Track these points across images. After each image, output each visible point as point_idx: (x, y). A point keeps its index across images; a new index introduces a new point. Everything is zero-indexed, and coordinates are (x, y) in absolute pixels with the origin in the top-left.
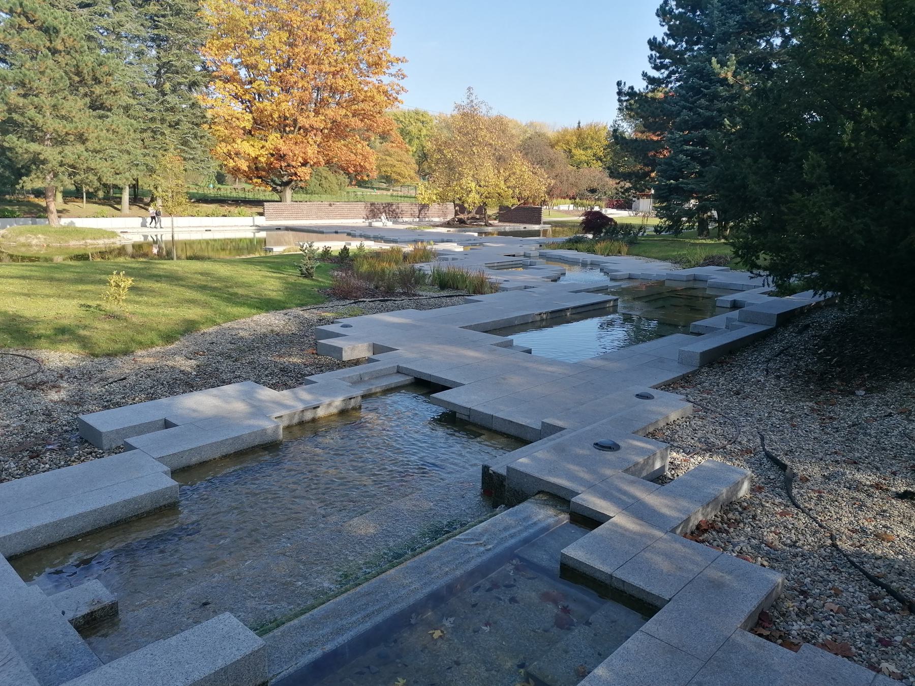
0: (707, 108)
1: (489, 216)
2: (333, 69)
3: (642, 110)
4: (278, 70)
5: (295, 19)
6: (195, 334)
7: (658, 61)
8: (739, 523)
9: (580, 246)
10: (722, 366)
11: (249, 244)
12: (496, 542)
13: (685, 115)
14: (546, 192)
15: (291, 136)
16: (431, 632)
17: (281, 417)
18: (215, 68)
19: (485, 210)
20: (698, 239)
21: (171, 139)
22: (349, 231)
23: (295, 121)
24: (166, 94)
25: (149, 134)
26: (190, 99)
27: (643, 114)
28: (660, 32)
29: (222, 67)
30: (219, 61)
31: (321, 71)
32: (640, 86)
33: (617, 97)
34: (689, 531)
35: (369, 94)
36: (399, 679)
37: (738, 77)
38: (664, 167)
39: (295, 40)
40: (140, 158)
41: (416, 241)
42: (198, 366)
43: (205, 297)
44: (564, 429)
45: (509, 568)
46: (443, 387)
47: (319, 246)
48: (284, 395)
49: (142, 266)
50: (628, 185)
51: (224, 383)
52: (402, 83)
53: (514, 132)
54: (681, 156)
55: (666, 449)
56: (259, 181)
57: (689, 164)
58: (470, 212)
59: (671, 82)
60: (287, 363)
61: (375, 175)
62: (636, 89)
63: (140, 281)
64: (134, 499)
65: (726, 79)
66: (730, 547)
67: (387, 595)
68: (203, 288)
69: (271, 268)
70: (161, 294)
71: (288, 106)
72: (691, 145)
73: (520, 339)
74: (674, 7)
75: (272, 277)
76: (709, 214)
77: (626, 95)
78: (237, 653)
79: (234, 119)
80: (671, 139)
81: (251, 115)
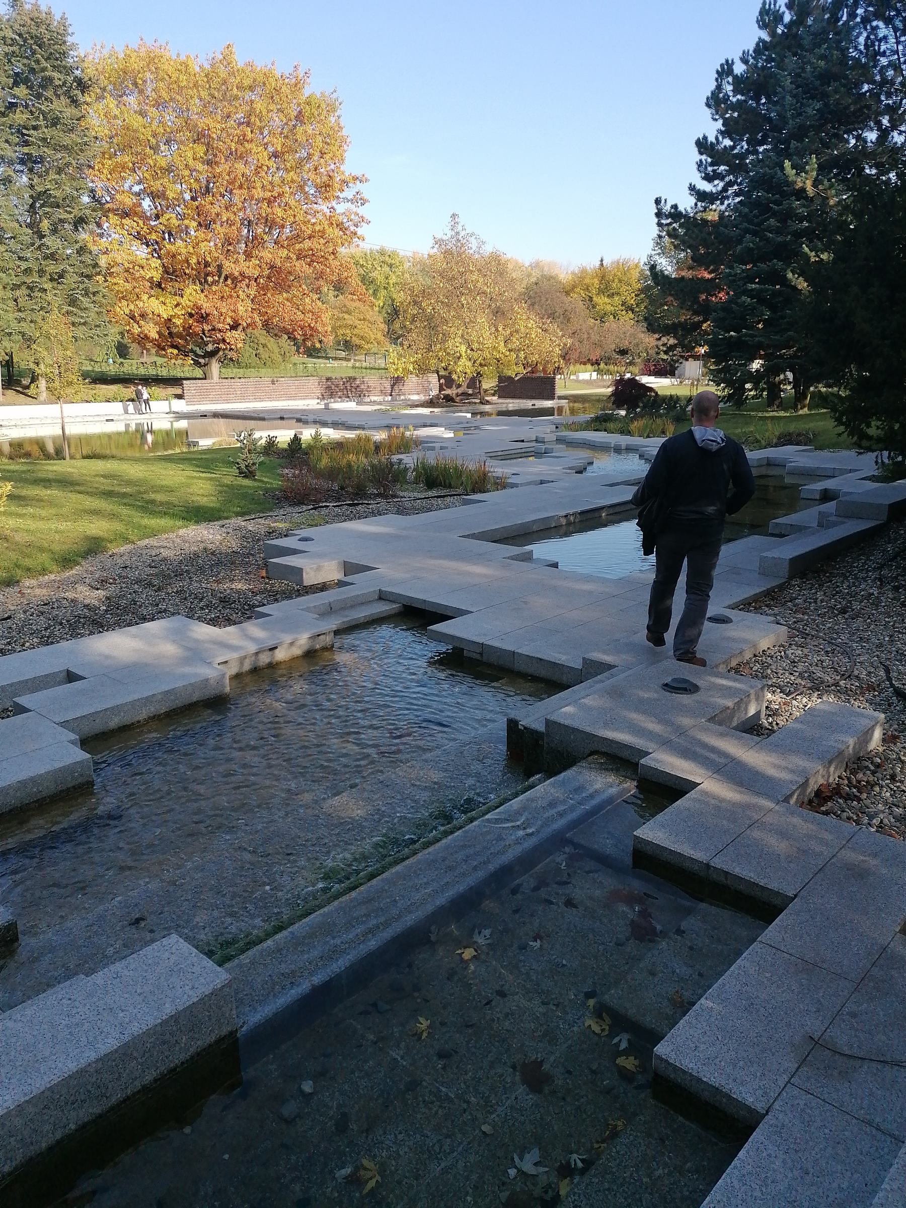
0: (778, 232)
1: (486, 391)
2: (268, 194)
3: (690, 237)
4: (193, 199)
5: (213, 124)
6: (100, 557)
7: (710, 169)
8: (872, 786)
9: (611, 425)
10: (819, 576)
11: (166, 438)
12: (540, 823)
13: (749, 241)
14: (561, 356)
15: (214, 288)
16: (459, 952)
17: (226, 662)
18: (108, 199)
19: (480, 382)
20: (767, 411)
21: (55, 297)
22: (298, 416)
23: (220, 267)
24: (44, 236)
25: (24, 291)
26: (76, 242)
27: (691, 242)
28: (711, 128)
29: (118, 196)
30: (113, 188)
31: (252, 198)
32: (687, 203)
33: (656, 220)
34: (806, 799)
35: (317, 228)
36: (421, 1019)
37: (820, 187)
38: (722, 314)
39: (215, 156)
40: (14, 324)
41: (388, 427)
42: (108, 598)
43: (111, 507)
44: (615, 666)
45: (560, 859)
46: (443, 616)
47: (262, 436)
48: (229, 633)
49: (25, 468)
50: (672, 341)
51: (144, 619)
52: (362, 211)
53: (514, 275)
54: (744, 298)
55: (762, 689)
56: (175, 351)
57: (755, 308)
58: (459, 386)
59: (728, 198)
60: (228, 591)
61: (330, 340)
62: (681, 208)
63: (22, 487)
64: (32, 780)
65: (803, 190)
66: (866, 820)
67: (395, 901)
68: (108, 494)
69: (197, 466)
70: (51, 503)
71: (209, 247)
72: (757, 283)
73: (542, 550)
74: (731, 94)
75: (200, 478)
76: (782, 377)
77: (667, 217)
78: (191, 993)
79: (137, 268)
80: (730, 275)
81: (159, 261)
